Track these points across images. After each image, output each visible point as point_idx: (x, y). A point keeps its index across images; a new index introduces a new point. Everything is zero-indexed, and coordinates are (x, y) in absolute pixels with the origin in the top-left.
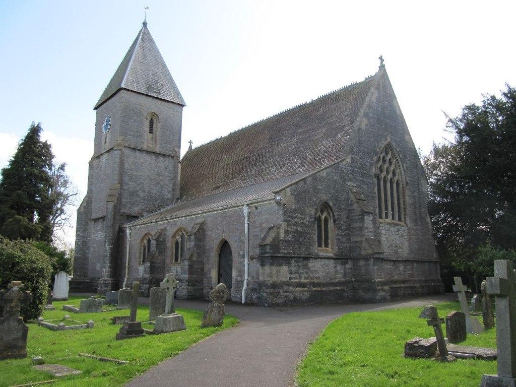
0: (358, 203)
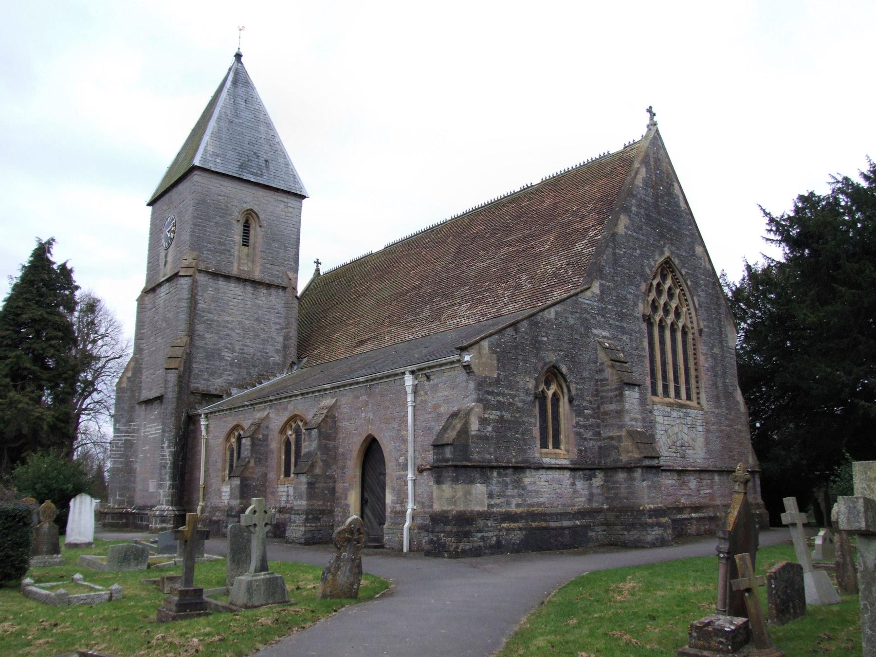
0: (613, 367)
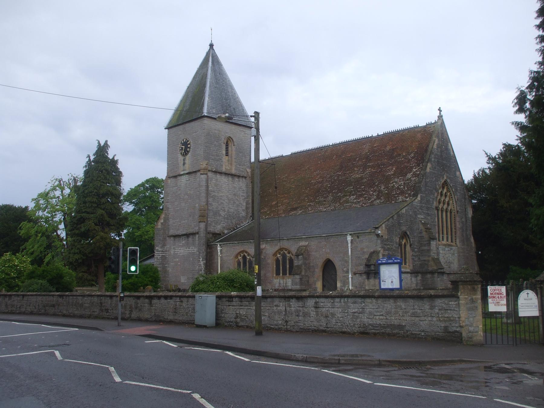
0: (426, 231)
